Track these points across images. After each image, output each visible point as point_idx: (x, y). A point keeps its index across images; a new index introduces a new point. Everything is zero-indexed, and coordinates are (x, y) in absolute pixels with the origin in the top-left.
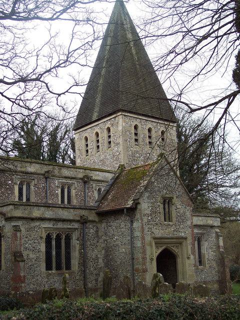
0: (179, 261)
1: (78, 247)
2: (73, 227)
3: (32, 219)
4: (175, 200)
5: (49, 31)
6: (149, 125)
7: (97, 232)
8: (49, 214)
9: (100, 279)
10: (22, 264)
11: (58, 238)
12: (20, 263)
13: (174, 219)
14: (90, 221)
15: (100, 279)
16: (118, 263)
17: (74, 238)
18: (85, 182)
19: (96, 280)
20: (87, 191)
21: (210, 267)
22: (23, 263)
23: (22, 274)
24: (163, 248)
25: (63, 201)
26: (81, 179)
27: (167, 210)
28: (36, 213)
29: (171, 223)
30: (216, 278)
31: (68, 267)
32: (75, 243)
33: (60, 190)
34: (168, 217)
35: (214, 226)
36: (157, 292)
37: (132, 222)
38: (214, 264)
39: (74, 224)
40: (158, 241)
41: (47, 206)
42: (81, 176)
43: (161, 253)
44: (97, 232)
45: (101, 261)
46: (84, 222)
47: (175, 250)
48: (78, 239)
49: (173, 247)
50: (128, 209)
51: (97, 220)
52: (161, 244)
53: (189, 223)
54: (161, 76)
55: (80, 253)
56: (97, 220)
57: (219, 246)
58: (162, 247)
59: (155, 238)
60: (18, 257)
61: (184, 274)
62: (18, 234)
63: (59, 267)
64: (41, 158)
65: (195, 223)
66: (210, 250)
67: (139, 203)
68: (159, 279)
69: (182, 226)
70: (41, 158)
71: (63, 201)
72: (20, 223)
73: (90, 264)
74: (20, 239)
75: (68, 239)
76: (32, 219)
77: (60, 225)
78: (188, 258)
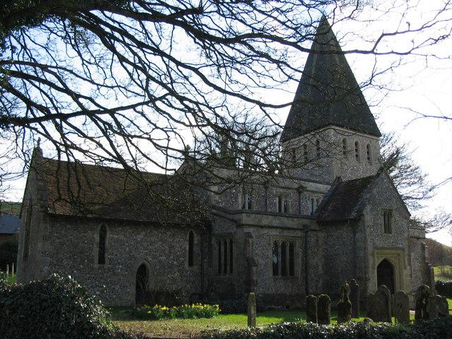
3: (262, 227)
5: (413, 49)
6: (356, 139)
8: (276, 222)
10: (254, 269)
11: (284, 244)
13: (393, 231)
15: (320, 285)
16: (339, 271)
17: (297, 246)
18: (300, 193)
19: (316, 286)
20: (301, 201)
23: (255, 279)
24: (383, 258)
25: (280, 210)
26: (296, 189)
27: (387, 222)
28: (266, 221)
31: (292, 272)
32: (298, 250)
33: (277, 200)
34: (388, 229)
36: (424, 302)
37: (355, 233)
39: (297, 231)
41: (266, 213)
45: (320, 268)
47: (393, 261)
50: (351, 220)
53: (406, 235)
54: (369, 94)
57: (424, 258)
60: (250, 263)
62: (250, 240)
63: (284, 274)
64: (279, 166)
65: (411, 234)
67: (363, 215)
68: (426, 291)
70: (279, 166)
71: (280, 210)
72: (251, 230)
75: (292, 247)
76: (262, 227)
77: (286, 233)
78: (405, 268)
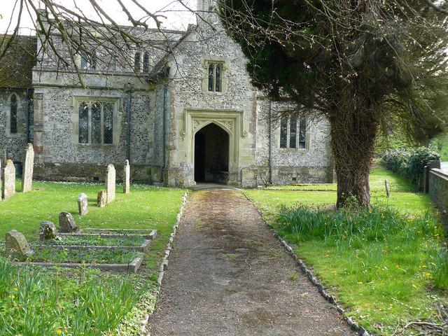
0: (231, 139)
1: (120, 119)
2: (114, 96)
4: (228, 65)
7: (148, 102)
9: (149, 155)
12: (37, 133)
14: (137, 90)
19: (144, 156)
21: (316, 150)
22: (41, 133)
24: (208, 122)
29: (218, 93)
30: (324, 164)
32: (118, 115)
35: (166, 92)
38: (323, 147)
39: (116, 92)
40: (197, 114)
42: (163, 38)
43: (203, 129)
44: (148, 102)
46: (129, 91)
48: (120, 110)
49: (224, 122)
51: (147, 88)
52: (204, 118)
55: (124, 126)
56: (147, 88)
58: (205, 121)
59: (190, 110)
61: (236, 154)
66: (319, 131)
69: (236, 98)
73: (135, 138)
74: (42, 108)
